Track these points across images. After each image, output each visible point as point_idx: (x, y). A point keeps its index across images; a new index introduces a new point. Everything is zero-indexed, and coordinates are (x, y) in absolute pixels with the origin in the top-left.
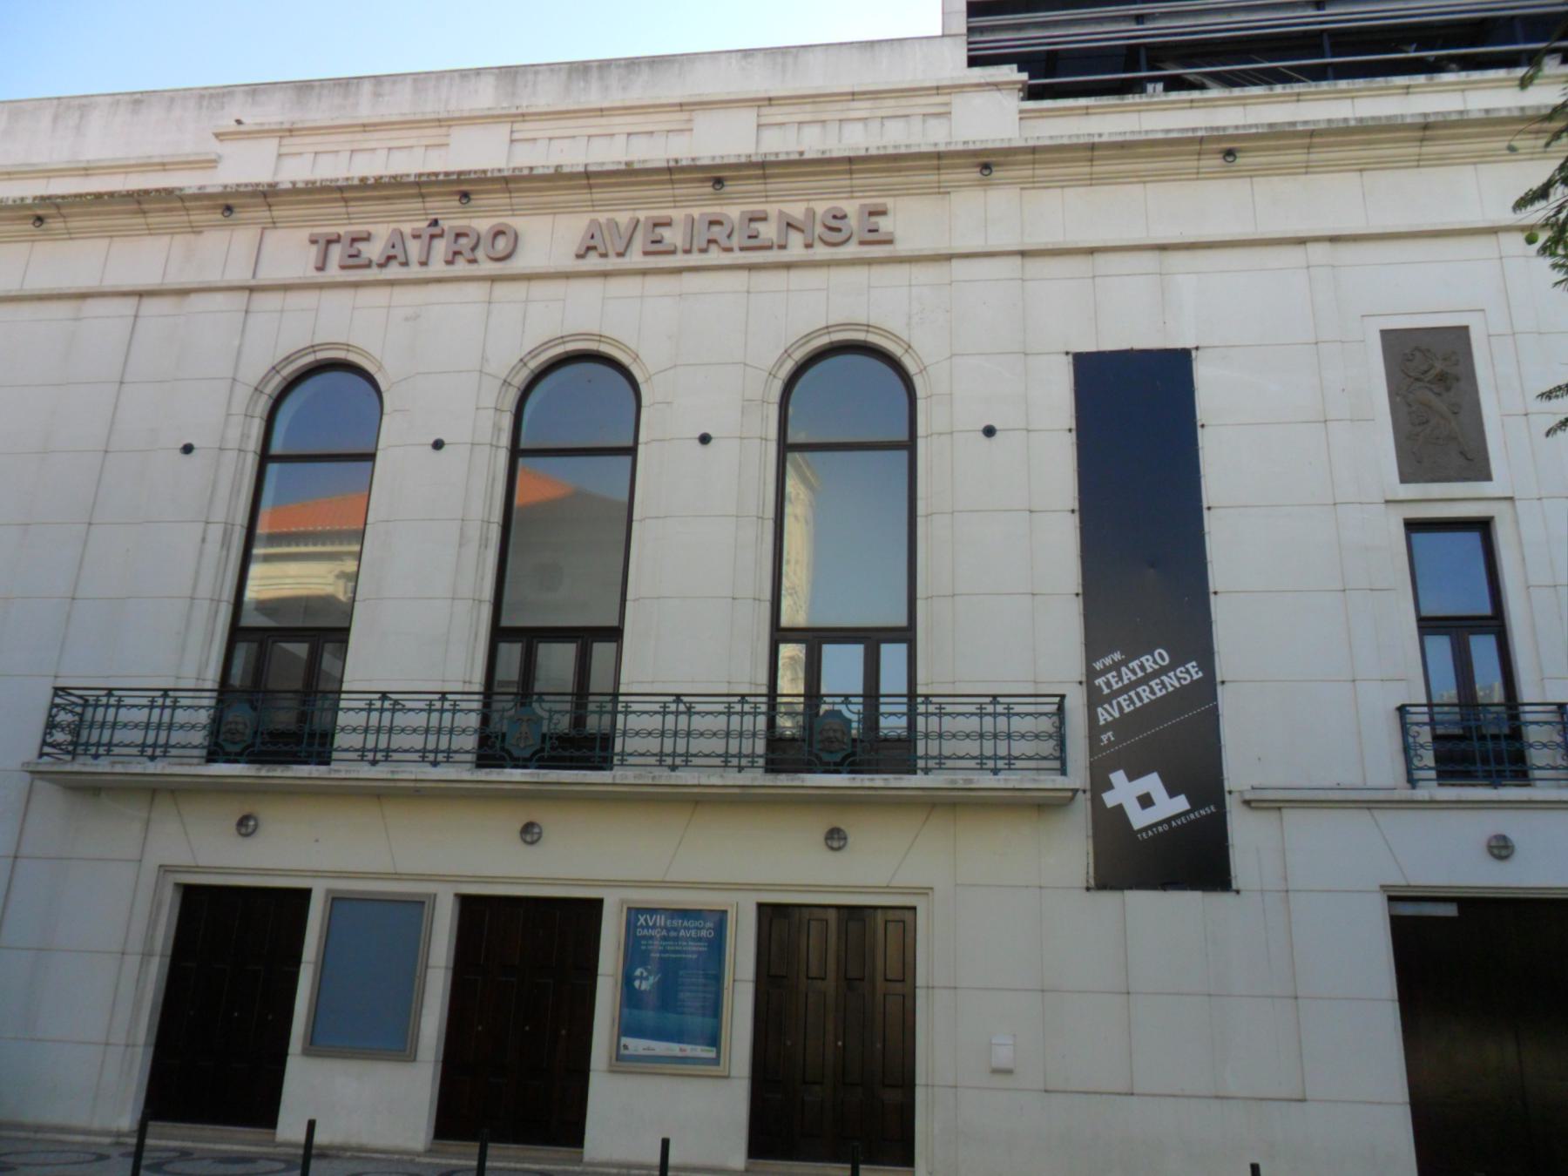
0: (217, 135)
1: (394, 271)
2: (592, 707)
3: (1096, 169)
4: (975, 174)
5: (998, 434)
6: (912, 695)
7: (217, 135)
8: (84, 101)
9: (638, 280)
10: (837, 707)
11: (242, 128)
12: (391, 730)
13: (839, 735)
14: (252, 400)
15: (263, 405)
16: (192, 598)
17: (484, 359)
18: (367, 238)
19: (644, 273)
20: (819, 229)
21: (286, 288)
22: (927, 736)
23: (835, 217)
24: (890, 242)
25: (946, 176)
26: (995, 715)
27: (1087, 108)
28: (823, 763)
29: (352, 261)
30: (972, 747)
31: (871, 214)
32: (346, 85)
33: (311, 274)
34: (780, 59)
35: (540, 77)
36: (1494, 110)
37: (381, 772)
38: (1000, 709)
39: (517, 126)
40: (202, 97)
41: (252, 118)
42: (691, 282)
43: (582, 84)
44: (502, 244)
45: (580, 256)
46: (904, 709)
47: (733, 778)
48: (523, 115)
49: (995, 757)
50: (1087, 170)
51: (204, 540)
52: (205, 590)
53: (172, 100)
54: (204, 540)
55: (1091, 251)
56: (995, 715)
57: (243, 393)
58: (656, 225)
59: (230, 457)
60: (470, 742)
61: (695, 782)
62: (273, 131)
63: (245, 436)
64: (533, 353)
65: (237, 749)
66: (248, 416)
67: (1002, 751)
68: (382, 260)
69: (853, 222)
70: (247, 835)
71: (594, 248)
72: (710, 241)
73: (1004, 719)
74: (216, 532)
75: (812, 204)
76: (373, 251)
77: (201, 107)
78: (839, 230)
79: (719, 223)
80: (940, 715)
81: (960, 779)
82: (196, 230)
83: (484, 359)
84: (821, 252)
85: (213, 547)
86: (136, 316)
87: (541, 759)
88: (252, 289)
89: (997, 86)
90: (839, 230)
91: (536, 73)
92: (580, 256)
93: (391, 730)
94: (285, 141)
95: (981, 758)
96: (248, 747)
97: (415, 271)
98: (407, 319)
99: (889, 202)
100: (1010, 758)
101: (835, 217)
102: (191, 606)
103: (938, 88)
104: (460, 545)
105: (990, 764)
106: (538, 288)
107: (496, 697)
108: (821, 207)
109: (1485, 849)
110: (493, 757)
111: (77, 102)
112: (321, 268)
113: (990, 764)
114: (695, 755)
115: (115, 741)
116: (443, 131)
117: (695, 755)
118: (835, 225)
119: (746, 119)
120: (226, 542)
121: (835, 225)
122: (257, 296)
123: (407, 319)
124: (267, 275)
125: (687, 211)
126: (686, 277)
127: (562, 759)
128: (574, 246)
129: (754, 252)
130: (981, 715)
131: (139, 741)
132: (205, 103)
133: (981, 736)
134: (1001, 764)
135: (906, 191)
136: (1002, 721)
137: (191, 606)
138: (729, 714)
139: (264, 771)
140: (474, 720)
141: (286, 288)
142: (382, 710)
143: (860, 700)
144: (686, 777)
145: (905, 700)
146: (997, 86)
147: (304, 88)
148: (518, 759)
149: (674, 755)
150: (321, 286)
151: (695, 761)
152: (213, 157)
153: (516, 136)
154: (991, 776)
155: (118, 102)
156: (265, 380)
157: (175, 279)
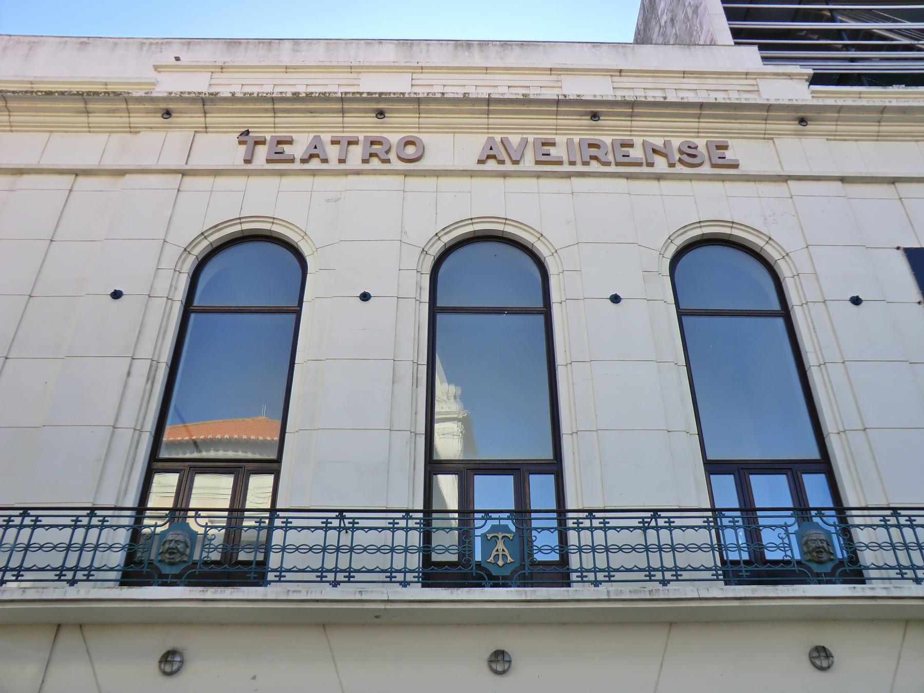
0: (156, 68)
1: (315, 164)
2: (570, 523)
3: (882, 128)
4: (795, 126)
5: (863, 304)
6: (561, 511)
7: (156, 68)
8: (86, 40)
9: (534, 181)
10: (503, 522)
11: (178, 63)
12: (96, 547)
13: (825, 545)
14: (181, 259)
15: (189, 264)
16: (114, 428)
17: (403, 232)
18: (290, 142)
19: (538, 175)
20: (677, 156)
21: (216, 173)
22: (580, 549)
23: (689, 147)
24: (736, 166)
25: (772, 126)
26: (592, 529)
27: (860, 93)
28: (162, 576)
29: (278, 157)
30: (640, 560)
31: (544, 144)
32: (268, 43)
33: (239, 163)
34: (621, 50)
35: (432, 48)
36: (386, 93)
37: (345, 592)
38: (596, 523)
39: (415, 76)
40: (143, 44)
41: (187, 58)
42: (578, 183)
43: (467, 53)
44: (410, 151)
45: (480, 162)
46: (554, 524)
47: (396, 592)
48: (422, 68)
49: (595, 570)
50: (876, 128)
51: (129, 374)
52: (128, 419)
53: (116, 44)
54: (129, 374)
55: (893, 181)
56: (592, 529)
57: (172, 255)
58: (279, 143)
59: (158, 304)
60: (117, 558)
61: (695, 595)
62: (208, 67)
63: (173, 287)
64: (446, 230)
65: (176, 570)
66: (177, 271)
67: (602, 564)
68: (306, 157)
69: (702, 149)
70: (811, 658)
71: (317, 156)
72: (371, 155)
73: (602, 533)
74: (141, 368)
75: (525, 136)
76: (298, 150)
77: (141, 49)
78: (694, 156)
79: (380, 143)
80: (605, 529)
81: (626, 591)
82: (133, 130)
83: (403, 232)
84: (680, 169)
85: (138, 381)
86: (70, 191)
87: (523, 577)
88: (184, 173)
89: (790, 76)
90: (694, 156)
91: (248, 43)
92: (480, 162)
93: (96, 547)
94: (215, 75)
95: (322, 571)
96: (187, 568)
97: (333, 164)
98: (328, 201)
99: (730, 142)
100: (609, 570)
101: (689, 147)
102: (113, 433)
103: (747, 74)
104: (393, 382)
105: (330, 577)
106: (444, 182)
107: (434, 515)
108: (676, 142)
109: (503, 649)
110: (139, 575)
111: (28, 39)
112: (247, 161)
113: (330, 577)
114: (290, 571)
115: (26, 565)
116: (354, 75)
117: (290, 571)
118: (689, 155)
119: (547, 79)
120: (151, 377)
121: (689, 155)
122: (188, 180)
123: (328, 201)
124: (196, 162)
125: (568, 135)
126: (574, 180)
127: (229, 575)
128: (477, 154)
129: (626, 166)
130: (326, 529)
131: (58, 564)
132: (145, 48)
133: (392, 550)
134: (600, 576)
135: (741, 135)
136: (599, 534)
137: (113, 433)
138: (645, 529)
139: (211, 593)
140: (123, 537)
141: (216, 173)
142: (89, 527)
143: (833, 513)
144: (676, 590)
145: (555, 515)
146: (790, 76)
147: (233, 43)
148: (497, 578)
149: (336, 571)
150: (249, 173)
151: (289, 576)
152: (153, 81)
153: (415, 82)
154: (592, 587)
155: (66, 42)
156: (194, 243)
157: (110, 162)
